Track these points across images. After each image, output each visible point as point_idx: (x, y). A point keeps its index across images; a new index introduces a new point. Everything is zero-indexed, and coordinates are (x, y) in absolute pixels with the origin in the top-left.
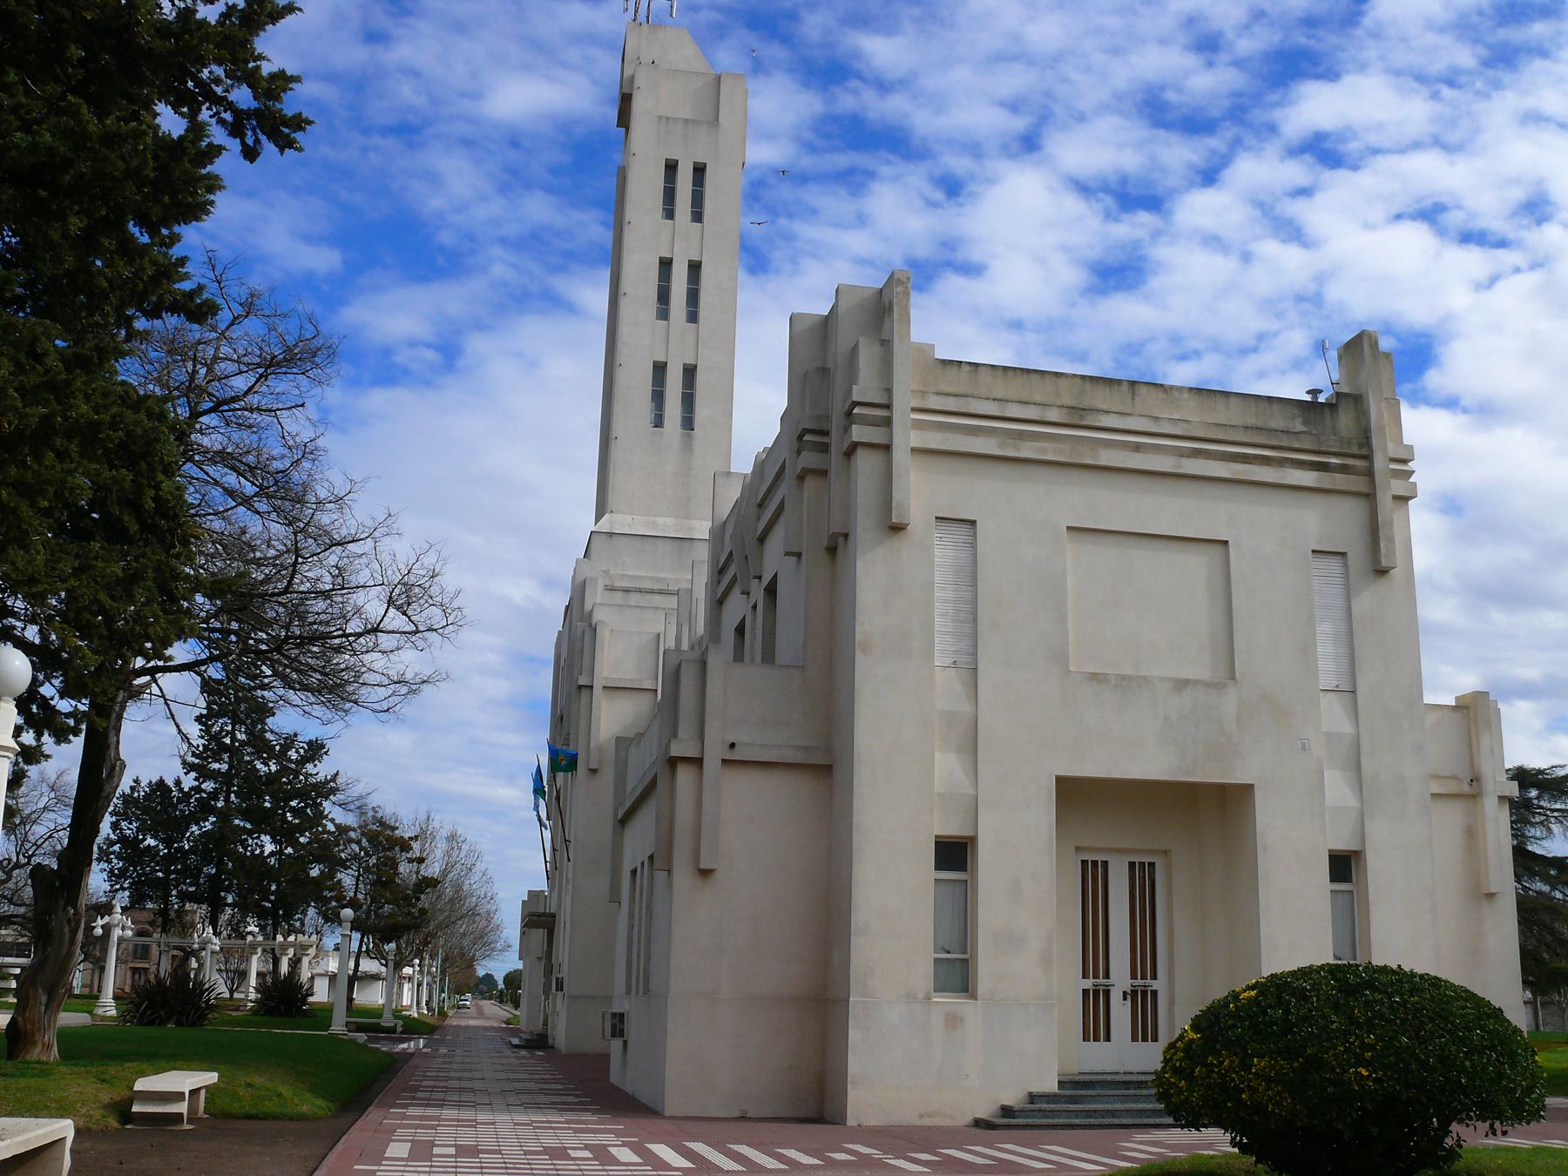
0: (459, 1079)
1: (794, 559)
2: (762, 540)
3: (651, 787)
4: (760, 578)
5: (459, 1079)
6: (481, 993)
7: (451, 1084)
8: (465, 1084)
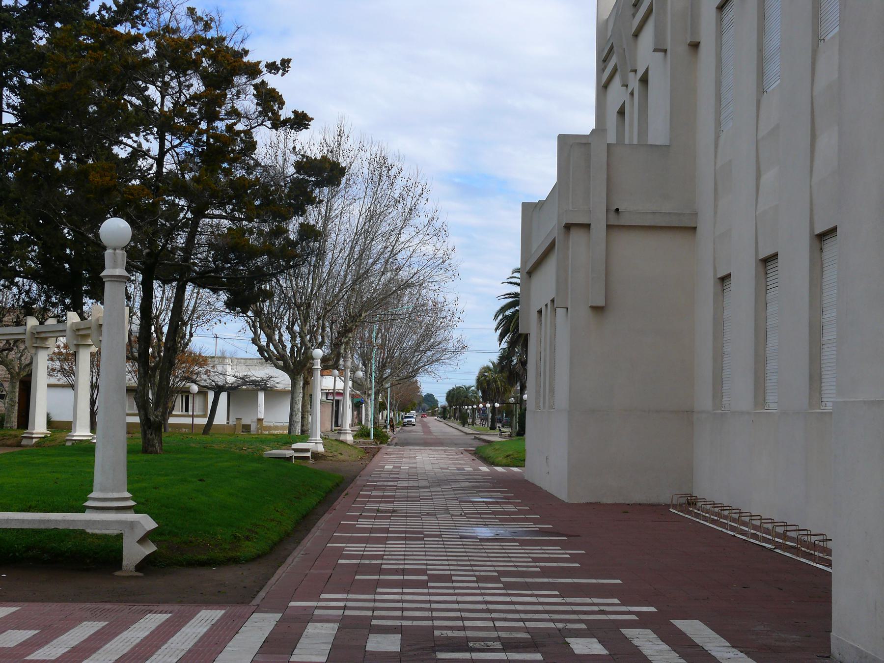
0: (407, 488)
1: (662, 54)
2: (636, 35)
3: (551, 247)
4: (635, 71)
5: (407, 488)
6: (423, 410)
7: (399, 493)
8: (413, 493)
